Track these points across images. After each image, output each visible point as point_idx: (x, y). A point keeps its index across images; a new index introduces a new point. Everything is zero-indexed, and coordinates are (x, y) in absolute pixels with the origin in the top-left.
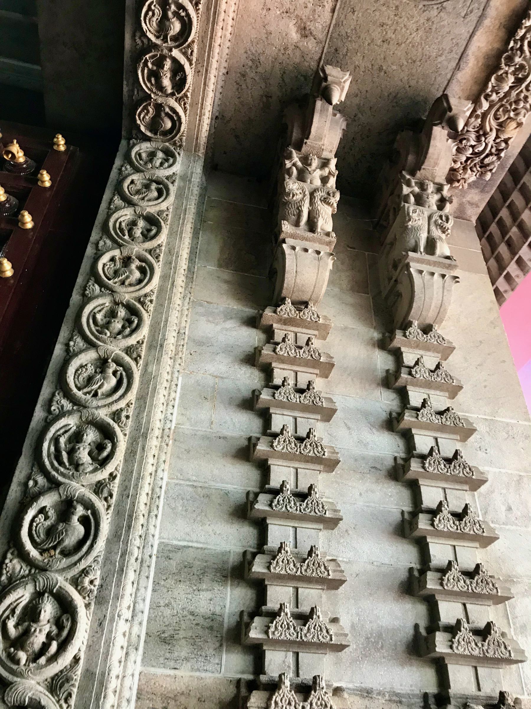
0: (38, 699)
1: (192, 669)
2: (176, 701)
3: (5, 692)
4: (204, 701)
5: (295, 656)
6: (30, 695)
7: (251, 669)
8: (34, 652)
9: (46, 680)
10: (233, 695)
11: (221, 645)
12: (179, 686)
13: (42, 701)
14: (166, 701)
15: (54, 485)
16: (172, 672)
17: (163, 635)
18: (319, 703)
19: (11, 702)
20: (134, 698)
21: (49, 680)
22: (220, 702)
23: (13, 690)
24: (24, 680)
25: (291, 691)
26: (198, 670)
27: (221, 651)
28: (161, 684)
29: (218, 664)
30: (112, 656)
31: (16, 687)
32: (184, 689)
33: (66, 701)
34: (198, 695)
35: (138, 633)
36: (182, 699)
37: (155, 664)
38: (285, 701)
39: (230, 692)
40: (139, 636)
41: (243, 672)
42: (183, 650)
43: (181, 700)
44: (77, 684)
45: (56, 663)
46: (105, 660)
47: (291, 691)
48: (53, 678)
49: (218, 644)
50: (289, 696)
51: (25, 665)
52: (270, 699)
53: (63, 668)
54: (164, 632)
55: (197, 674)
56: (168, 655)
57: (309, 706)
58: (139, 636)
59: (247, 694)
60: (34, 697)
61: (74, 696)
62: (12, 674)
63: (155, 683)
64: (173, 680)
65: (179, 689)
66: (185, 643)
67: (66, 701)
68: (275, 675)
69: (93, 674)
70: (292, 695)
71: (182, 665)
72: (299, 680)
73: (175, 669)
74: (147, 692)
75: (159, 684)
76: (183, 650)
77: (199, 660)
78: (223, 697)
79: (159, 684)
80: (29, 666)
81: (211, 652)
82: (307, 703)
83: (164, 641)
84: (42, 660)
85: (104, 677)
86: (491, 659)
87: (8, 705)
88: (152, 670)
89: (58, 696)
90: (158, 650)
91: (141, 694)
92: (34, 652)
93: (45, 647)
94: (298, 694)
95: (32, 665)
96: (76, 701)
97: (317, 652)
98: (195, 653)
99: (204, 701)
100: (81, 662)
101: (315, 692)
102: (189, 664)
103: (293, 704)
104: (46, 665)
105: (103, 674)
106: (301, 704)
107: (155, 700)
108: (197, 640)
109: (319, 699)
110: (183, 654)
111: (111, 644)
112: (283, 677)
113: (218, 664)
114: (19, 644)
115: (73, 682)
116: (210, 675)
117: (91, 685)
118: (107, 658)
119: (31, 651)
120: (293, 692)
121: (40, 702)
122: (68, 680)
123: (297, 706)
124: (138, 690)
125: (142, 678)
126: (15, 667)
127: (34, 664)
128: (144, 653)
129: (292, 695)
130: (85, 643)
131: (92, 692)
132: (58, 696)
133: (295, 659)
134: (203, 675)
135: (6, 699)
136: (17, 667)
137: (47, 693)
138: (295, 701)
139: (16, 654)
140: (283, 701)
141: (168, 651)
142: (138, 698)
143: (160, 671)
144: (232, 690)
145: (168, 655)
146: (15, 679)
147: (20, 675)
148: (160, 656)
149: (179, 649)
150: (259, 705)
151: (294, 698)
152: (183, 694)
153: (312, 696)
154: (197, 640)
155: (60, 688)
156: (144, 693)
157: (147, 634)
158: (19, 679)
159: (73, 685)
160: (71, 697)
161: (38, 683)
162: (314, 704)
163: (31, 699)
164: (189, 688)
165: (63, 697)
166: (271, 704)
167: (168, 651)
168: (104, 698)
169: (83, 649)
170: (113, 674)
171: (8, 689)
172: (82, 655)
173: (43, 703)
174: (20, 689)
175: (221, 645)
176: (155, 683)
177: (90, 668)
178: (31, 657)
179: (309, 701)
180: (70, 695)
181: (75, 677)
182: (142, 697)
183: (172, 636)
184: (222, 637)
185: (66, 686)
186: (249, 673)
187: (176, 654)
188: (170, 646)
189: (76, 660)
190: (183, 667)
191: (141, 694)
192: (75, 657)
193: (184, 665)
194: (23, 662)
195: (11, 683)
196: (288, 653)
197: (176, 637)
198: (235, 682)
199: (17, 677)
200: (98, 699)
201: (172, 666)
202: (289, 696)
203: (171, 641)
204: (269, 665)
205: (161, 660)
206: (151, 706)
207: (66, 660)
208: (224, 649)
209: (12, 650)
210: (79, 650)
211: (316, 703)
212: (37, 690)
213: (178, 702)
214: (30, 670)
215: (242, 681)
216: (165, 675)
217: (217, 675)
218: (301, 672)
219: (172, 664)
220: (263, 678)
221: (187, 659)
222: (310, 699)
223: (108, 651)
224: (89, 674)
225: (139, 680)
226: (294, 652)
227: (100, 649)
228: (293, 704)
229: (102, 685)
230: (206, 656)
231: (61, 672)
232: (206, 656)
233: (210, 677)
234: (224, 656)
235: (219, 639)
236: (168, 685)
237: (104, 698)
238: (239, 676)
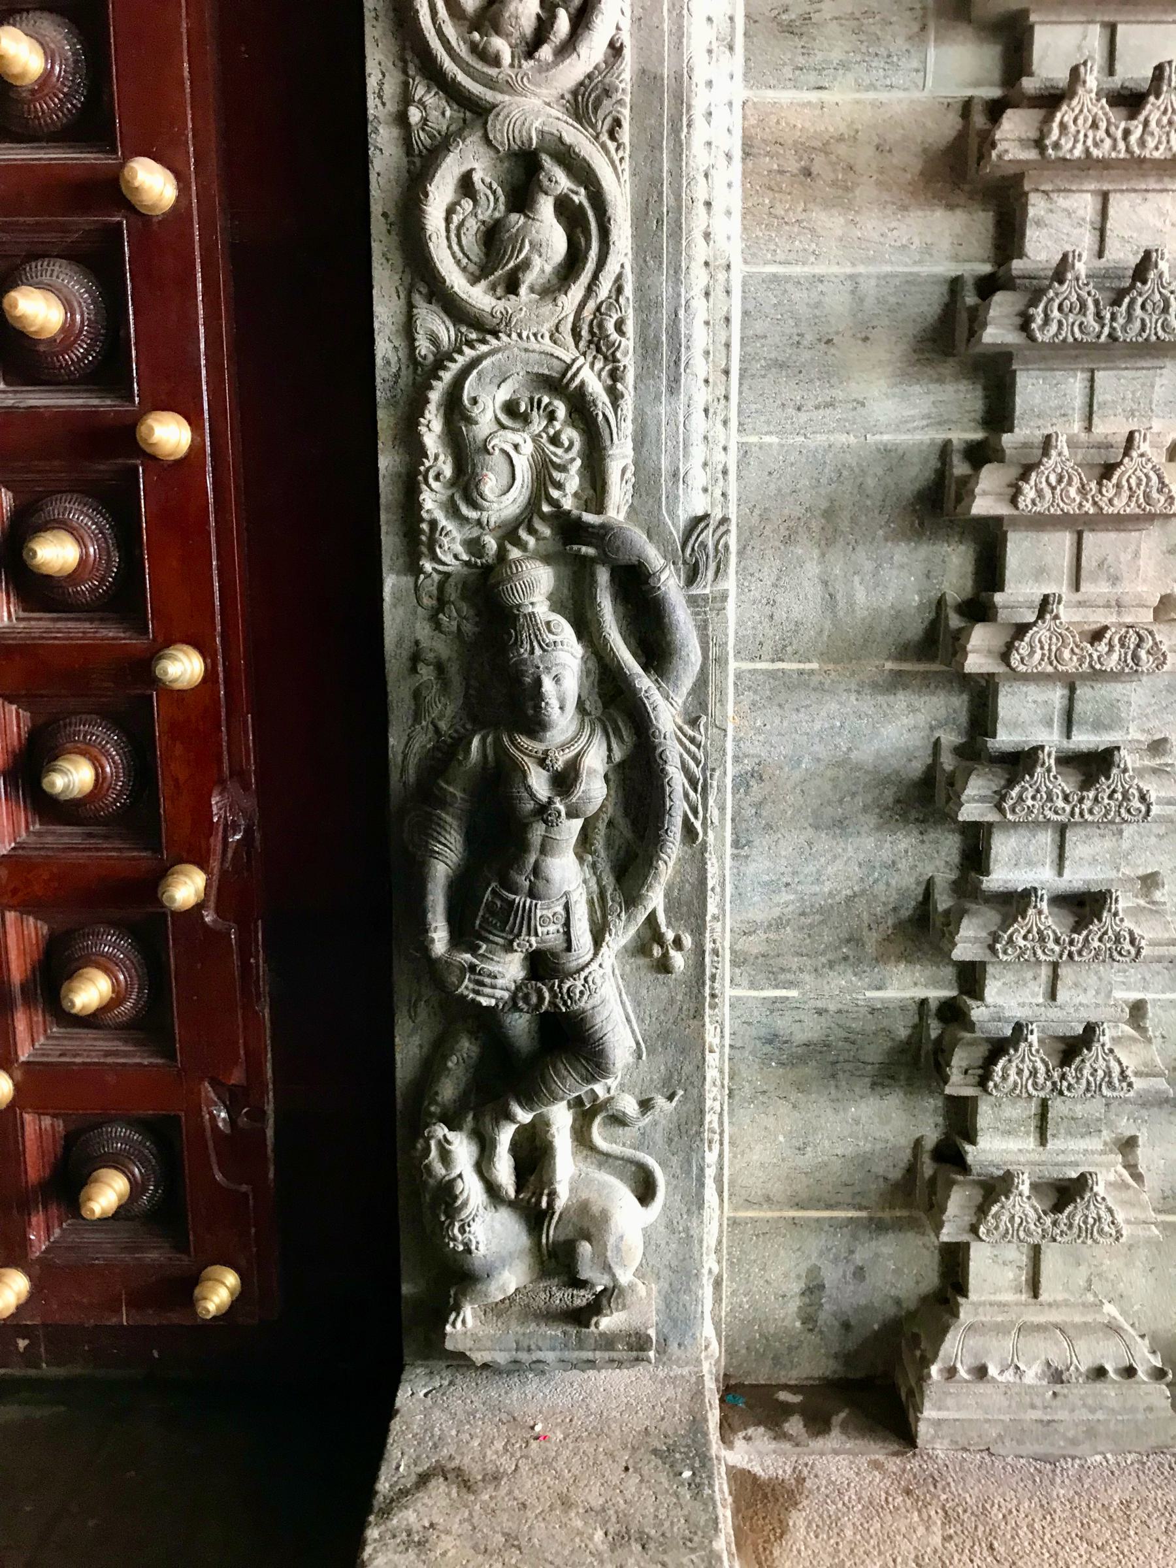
0: (556, 132)
1: (859, 87)
2: (827, 154)
3: (486, 123)
4: (890, 151)
5: (1108, 32)
6: (537, 124)
7: (996, 75)
8: (523, 36)
9: (562, 97)
10: (954, 133)
11: (923, 28)
12: (833, 125)
13: (564, 134)
14: (805, 156)
15: (476, 112)
16: (813, 97)
17: (784, 17)
18: (1165, 120)
19: (502, 144)
20: (737, 154)
21: (568, 96)
22: (925, 150)
23: (501, 118)
24: (517, 98)
25: (1098, 100)
26: (872, 87)
27: (924, 42)
28: (793, 122)
29: (917, 71)
30: (689, 38)
31: (505, 111)
32: (843, 128)
33: (612, 136)
34: (876, 140)
35: (729, 13)
36: (842, 150)
37: (772, 82)
38: (1085, 121)
39: (948, 126)
40: (731, 19)
41: (977, 84)
42: (834, 46)
43: (839, 152)
44: (627, 99)
45: (575, 56)
46: (678, 46)
47: (1098, 100)
48: (575, 93)
49: (916, 27)
50: (1095, 110)
51: (512, 66)
52: (1048, 120)
53: (589, 69)
54: (786, 11)
55: (871, 95)
56: (801, 61)
57: (1141, 127)
58: (731, 19)
59: (987, 127)
60: (546, 129)
61: (626, 124)
62: (491, 88)
63: (778, 122)
64: (818, 112)
65: (832, 130)
66: (838, 29)
67: (612, 136)
68: (1061, 76)
69: (657, 78)
70: (1102, 108)
71: (835, 79)
72: (1116, 82)
73: (820, 88)
74: (764, 141)
75: (787, 124)
76: (834, 46)
77: (874, 65)
78: (930, 140)
79: (787, 124)
80: (520, 67)
81: (901, 44)
82: (1135, 122)
83: (789, 30)
84: (546, 52)
85: (681, 83)
86: (1132, 345)
87: (498, 151)
88: (770, 95)
89: (593, 126)
90: (777, 50)
91: (751, 146)
92: (523, 36)
93: (543, 28)
94: (1115, 109)
95: (527, 65)
96: (632, 135)
97: (1165, 18)
98: (864, 50)
99: (890, 151)
100: (627, 52)
101: (1157, 97)
102: (850, 76)
103: (1103, 125)
104: (556, 63)
105: (678, 78)
106: (1123, 125)
107: (784, 156)
108: (865, 21)
109: (1165, 112)
110: (836, 55)
111: (685, 12)
112: (1082, 69)
113: (917, 71)
114: (487, 23)
115: (619, 96)
116: (901, 95)
117: (656, 103)
118: (681, 42)
119: (517, 34)
120: (1104, 101)
121: (560, 138)
122: (607, 93)
123: (1112, 129)
124: (744, 137)
125: (748, 112)
126: (493, 72)
127: (532, 63)
128: (747, 60)
129: (1102, 108)
130: (628, 12)
131: (661, 116)
132: (593, 126)
133: (1106, 40)
134: (884, 96)
135: (491, 137)
136: (497, 70)
137: (570, 121)
138: (1108, 121)
139: (488, 43)
140: (1080, 121)
141: (800, 50)
142: (746, 154)
143: (785, 96)
144: (951, 124)
145: (801, 61)
146: (499, 97)
147: (509, 87)
148: (784, 64)
149: (826, 45)
150: (1024, 136)
151: (1105, 114)
152: (841, 139)
153: (1149, 107)
154: (865, 21)
155: (596, 109)
156: (756, 142)
157: (747, 16)
158: (507, 98)
159: (620, 102)
160: (619, 125)
161: (549, 104)
162: (1153, 124)
163: (541, 133)
164: (855, 127)
165: (606, 128)
166: (1050, 131)
167: (800, 50)
168: (689, 126)
169: (626, 24)
170: (699, 77)
171: (491, 117)
172: (626, 38)
173: (568, 139)
174: (516, 114)
175: (923, 28)
176: (778, 122)
177: (649, 67)
178: (518, 51)
179: (1141, 118)
180: (617, 123)
181: (622, 86)
182: (755, 151)
183: (807, 18)
184: (924, 8)
185: (607, 103)
186: (992, 85)
187: (820, 56)
188: (804, 38)
189: (615, 50)
190: (836, 84)
191: (751, 146)
192: (611, 45)
193: (839, 79)
194: (506, 58)
195: (494, 106)
196: (1091, 27)
197: (816, 17)
198: (958, 107)
199: (502, 92)
200: (676, 131)
201: (813, 84)
202: (1095, 110)
203: (804, 29)
204: (1042, 59)
205: (787, 71)
206: (775, 167)
207: (592, 50)
208: (932, 37)
209: (476, 36)
210: (618, 28)
211: (1158, 122)
212: (549, 116)
213: (833, 158)
214: (526, 74)
215: (976, 101)
216: (799, 105)
217: (916, 95)
218: (1118, 67)
219: (812, 78)
220: (1029, 84)
221: (844, 66)
222: (1144, 113)
223: (680, 27)
224: (648, 80)
225: (744, 118)
226: (1104, 25)
227: (662, 22)
228: (1103, 125)
229: (680, 99)
230: (889, 56)
231: (589, 76)
232: (889, 56)
233: (900, 101)
234: (932, 52)
235: (919, 13)
236: (808, 125)
237: (689, 126)
238: (969, 92)
